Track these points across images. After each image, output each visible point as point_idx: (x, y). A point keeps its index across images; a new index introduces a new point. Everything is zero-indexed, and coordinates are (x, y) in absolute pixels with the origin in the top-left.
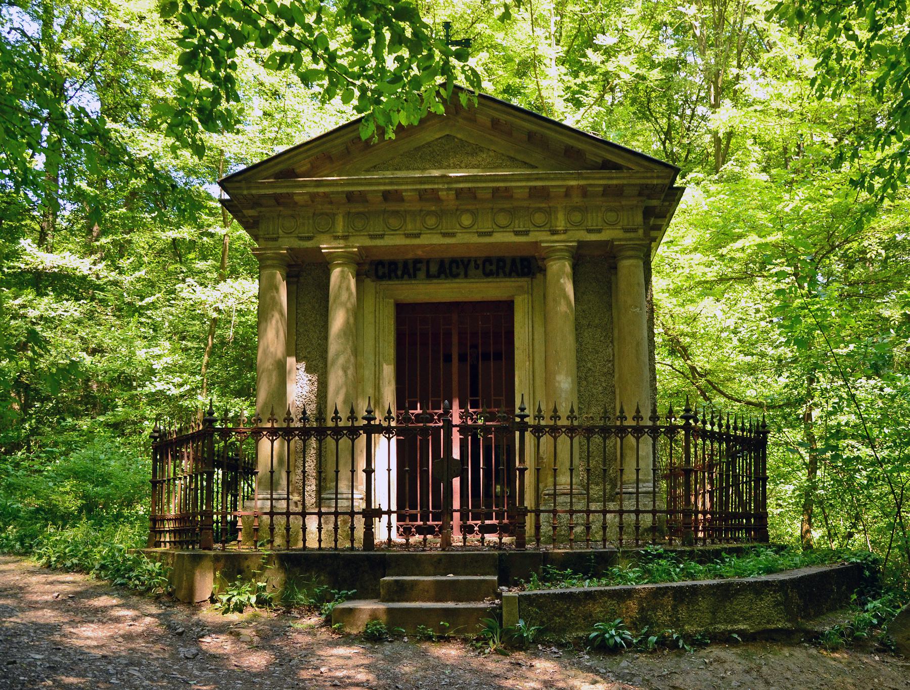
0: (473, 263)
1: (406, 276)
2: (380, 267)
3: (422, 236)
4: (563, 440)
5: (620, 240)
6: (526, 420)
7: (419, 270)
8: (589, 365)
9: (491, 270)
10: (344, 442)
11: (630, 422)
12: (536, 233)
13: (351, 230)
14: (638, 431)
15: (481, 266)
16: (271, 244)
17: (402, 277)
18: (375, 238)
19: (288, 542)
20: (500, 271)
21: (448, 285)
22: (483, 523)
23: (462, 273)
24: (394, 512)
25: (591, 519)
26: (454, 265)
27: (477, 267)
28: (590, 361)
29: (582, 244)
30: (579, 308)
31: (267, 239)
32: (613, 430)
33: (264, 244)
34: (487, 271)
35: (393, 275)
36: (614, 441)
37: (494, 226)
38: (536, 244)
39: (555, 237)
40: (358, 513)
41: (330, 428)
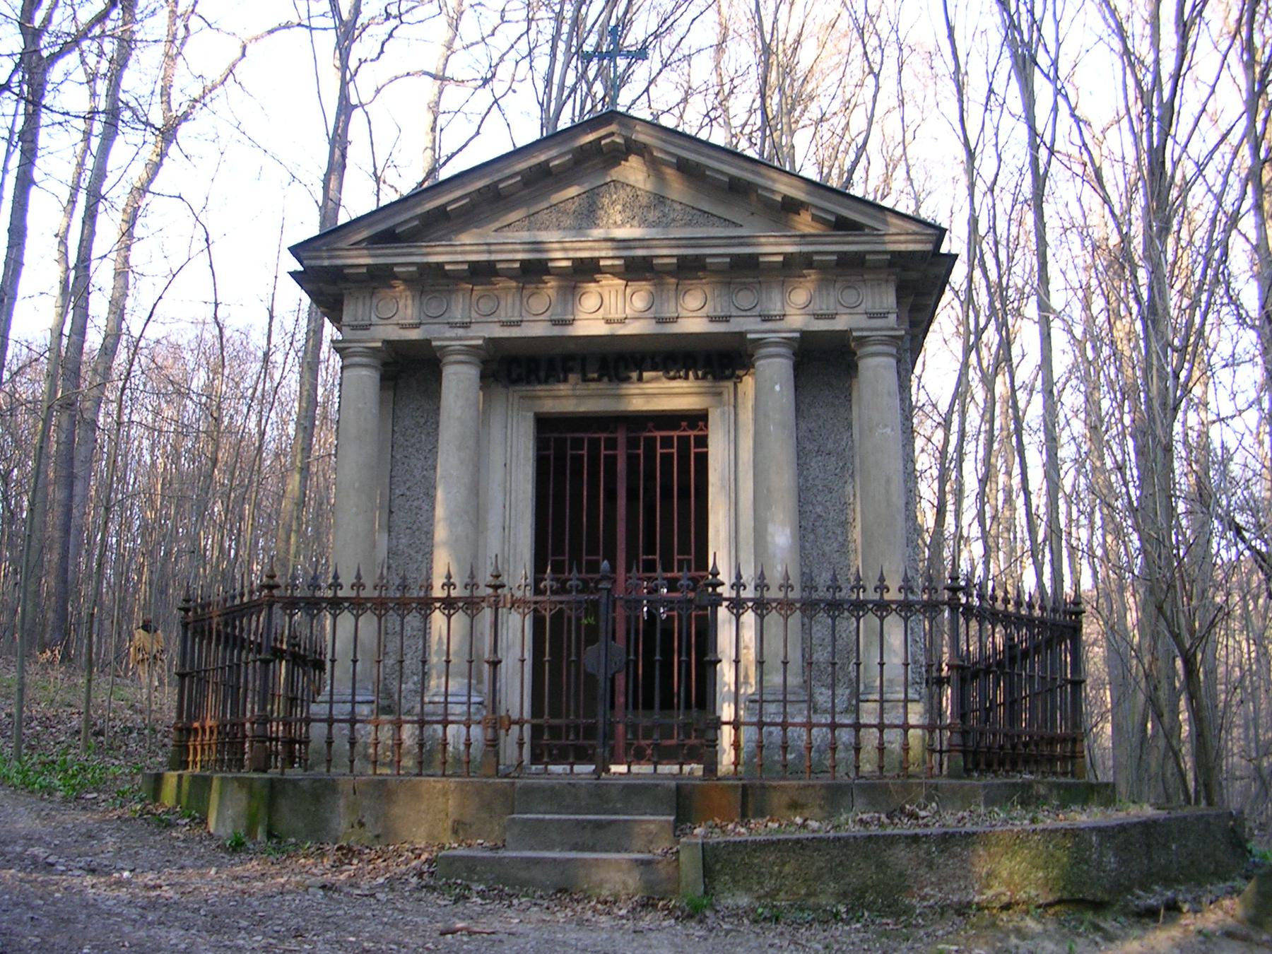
4: (773, 618)
5: (862, 330)
6: (719, 590)
8: (819, 509)
10: (413, 620)
11: (872, 595)
14: (882, 608)
16: (360, 334)
19: (421, 763)
24: (527, 722)
25: (789, 734)
28: (820, 503)
29: (491, 341)
30: (803, 426)
31: (354, 328)
33: (350, 334)
36: (847, 624)
38: (741, 335)
39: (768, 326)
40: (857, 736)
41: (438, 600)
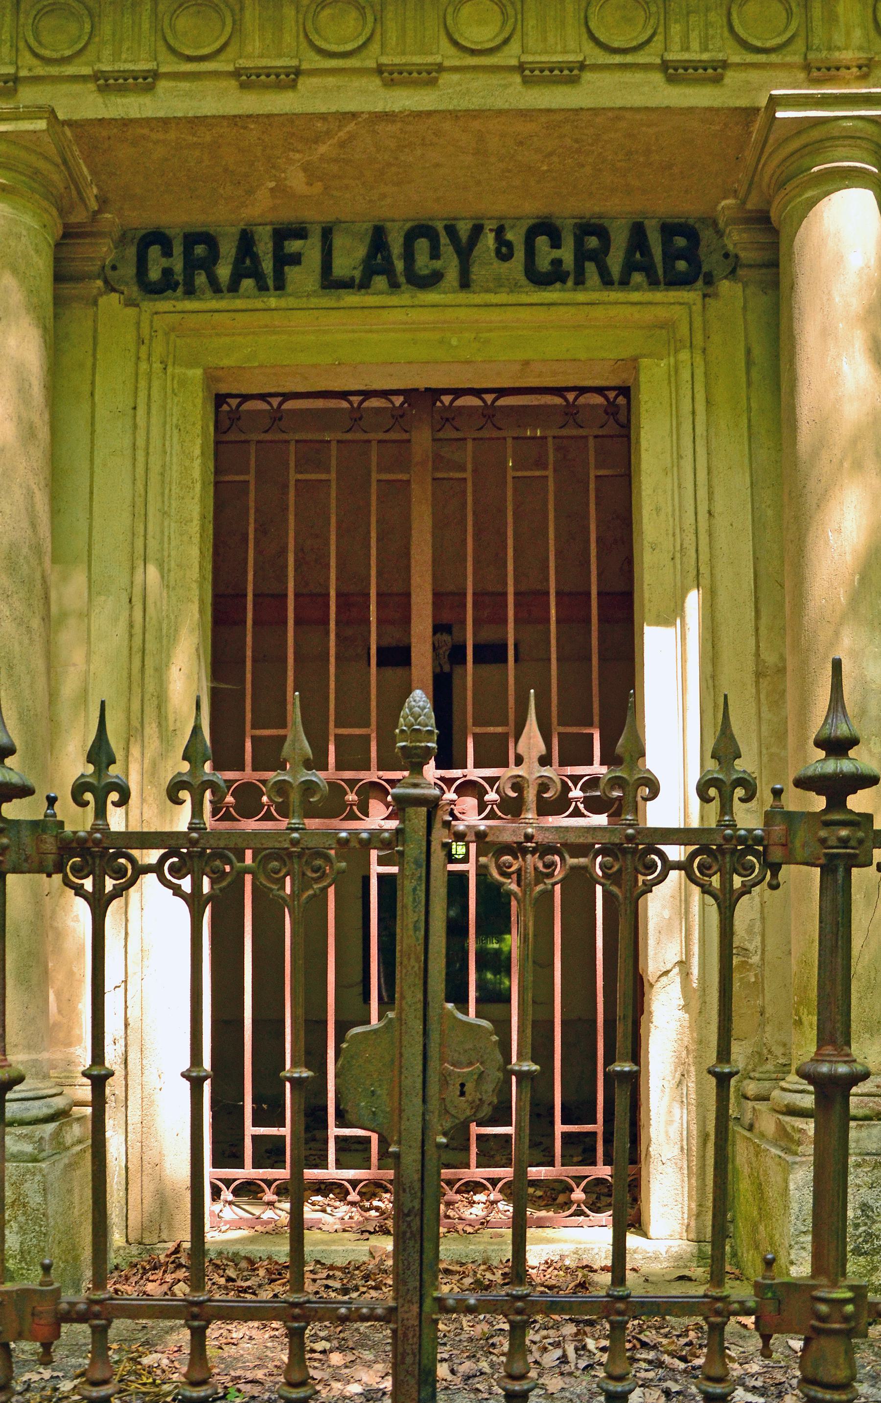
0: (489, 240)
1: (248, 283)
2: (154, 251)
3: (304, 83)
7: (296, 259)
9: (557, 263)
12: (754, 76)
13: (27, 58)
15: (520, 254)
17: (234, 287)
18: (122, 90)
20: (590, 267)
21: (398, 315)
22: (520, 1173)
23: (452, 275)
26: (422, 245)
27: (504, 252)
32: (675, 853)
34: (543, 264)
35: (201, 279)
37: (589, 47)
